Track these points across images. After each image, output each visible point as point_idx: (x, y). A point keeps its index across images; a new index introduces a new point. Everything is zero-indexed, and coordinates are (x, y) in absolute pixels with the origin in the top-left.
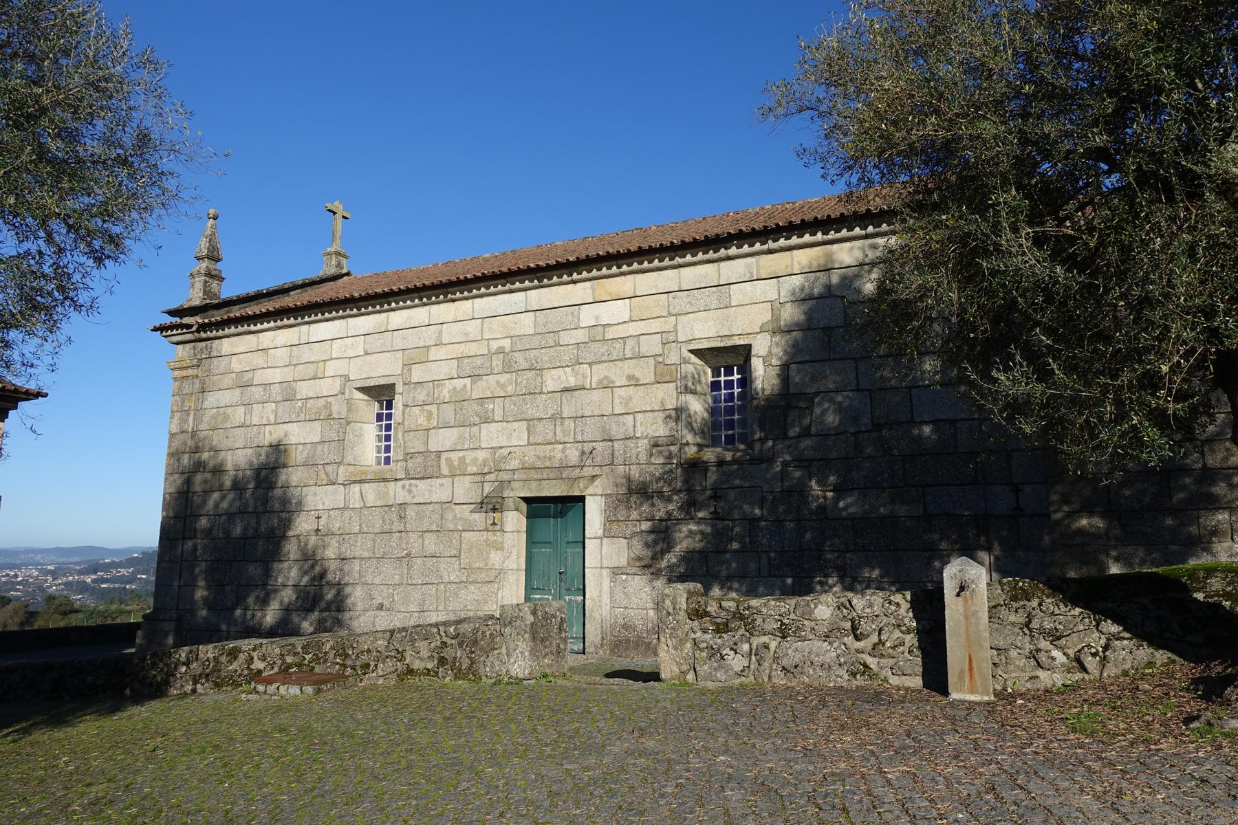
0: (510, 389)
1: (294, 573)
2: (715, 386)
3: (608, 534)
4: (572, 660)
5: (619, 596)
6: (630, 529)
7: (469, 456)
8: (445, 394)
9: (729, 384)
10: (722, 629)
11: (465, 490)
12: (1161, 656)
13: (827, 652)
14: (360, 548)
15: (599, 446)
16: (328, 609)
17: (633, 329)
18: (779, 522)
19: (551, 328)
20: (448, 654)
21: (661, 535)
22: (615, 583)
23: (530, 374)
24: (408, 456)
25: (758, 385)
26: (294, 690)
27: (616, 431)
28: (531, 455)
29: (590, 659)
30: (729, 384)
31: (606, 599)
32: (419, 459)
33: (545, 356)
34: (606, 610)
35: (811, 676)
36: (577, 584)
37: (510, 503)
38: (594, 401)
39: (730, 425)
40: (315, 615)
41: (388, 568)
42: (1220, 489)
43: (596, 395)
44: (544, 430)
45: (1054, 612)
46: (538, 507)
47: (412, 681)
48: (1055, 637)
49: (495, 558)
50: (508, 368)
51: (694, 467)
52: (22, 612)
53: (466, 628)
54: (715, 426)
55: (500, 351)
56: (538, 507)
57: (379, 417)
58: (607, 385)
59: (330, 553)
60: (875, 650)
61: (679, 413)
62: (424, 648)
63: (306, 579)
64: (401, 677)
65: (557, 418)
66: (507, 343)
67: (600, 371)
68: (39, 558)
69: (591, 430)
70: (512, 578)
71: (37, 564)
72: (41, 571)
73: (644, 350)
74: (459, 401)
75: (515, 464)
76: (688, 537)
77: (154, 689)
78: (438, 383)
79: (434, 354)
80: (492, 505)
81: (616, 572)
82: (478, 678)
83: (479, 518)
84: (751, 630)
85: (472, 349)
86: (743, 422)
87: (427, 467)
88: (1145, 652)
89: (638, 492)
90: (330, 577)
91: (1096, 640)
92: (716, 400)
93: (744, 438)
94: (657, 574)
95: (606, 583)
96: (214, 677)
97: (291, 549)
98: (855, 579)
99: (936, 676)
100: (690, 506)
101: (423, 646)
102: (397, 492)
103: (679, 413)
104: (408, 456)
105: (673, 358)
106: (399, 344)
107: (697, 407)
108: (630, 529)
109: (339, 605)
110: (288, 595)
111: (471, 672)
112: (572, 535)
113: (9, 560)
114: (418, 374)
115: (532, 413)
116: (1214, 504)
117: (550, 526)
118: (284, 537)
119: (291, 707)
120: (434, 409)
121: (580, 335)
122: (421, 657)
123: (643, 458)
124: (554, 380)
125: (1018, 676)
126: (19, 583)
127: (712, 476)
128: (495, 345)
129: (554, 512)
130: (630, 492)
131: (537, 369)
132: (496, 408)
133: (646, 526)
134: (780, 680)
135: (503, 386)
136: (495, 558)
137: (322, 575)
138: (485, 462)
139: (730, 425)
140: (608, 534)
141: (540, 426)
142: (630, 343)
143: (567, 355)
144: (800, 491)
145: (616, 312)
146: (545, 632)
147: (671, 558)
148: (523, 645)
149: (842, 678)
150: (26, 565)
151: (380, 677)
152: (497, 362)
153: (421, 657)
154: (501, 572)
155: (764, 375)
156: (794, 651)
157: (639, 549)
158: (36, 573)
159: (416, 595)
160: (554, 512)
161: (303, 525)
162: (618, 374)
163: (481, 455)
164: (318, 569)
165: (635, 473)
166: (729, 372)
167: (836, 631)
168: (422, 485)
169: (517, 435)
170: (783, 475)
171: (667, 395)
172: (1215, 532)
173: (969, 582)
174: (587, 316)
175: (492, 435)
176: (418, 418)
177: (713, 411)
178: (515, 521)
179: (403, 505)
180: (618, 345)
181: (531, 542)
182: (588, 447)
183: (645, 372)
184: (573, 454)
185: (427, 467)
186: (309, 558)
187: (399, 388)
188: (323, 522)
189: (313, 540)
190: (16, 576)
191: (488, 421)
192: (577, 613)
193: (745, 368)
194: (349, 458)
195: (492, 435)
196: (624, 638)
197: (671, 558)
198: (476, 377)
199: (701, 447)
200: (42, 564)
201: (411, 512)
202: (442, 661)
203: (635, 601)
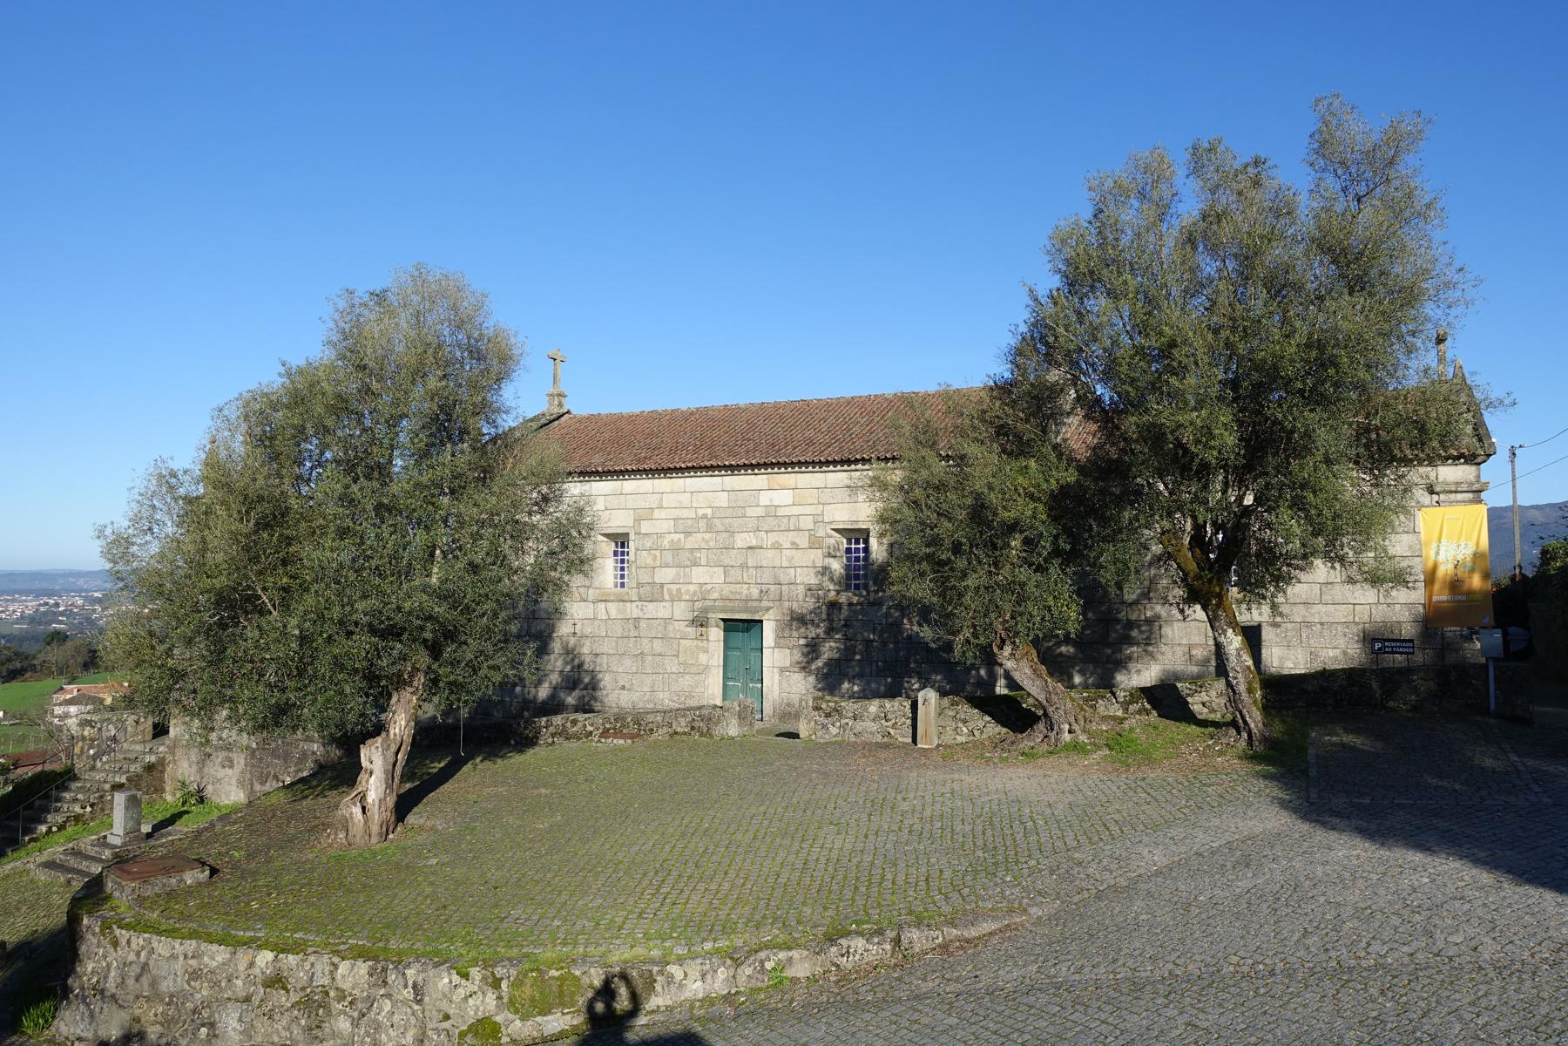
0: (712, 544)
1: (559, 663)
2: (848, 551)
3: (777, 646)
4: (758, 725)
5: (785, 685)
6: (793, 642)
7: (684, 588)
8: (666, 543)
9: (857, 550)
10: (828, 715)
11: (681, 611)
12: (1004, 730)
13: (874, 727)
14: (606, 647)
15: (772, 588)
16: (585, 688)
17: (796, 510)
18: (884, 643)
19: (740, 503)
20: (696, 724)
21: (812, 649)
22: (783, 677)
23: (725, 535)
24: (639, 585)
25: (873, 556)
26: (621, 742)
27: (783, 578)
28: (726, 590)
29: (767, 724)
30: (857, 550)
31: (776, 687)
32: (648, 588)
33: (736, 523)
34: (776, 694)
35: (866, 737)
36: (757, 676)
37: (712, 622)
38: (768, 558)
39: (857, 577)
40: (576, 693)
41: (627, 662)
42: (1135, 633)
43: (770, 554)
44: (735, 574)
45: (966, 710)
46: (731, 626)
47: (677, 737)
48: (965, 722)
49: (703, 658)
50: (710, 528)
51: (833, 606)
52: (84, 651)
53: (705, 712)
54: (848, 577)
55: (705, 516)
56: (731, 626)
57: (616, 553)
58: (777, 547)
59: (585, 650)
60: (893, 726)
61: (825, 570)
62: (683, 721)
63: (568, 668)
64: (671, 736)
65: (744, 566)
66: (709, 512)
67: (773, 537)
68: (81, 582)
69: (767, 577)
70: (714, 671)
71: (81, 590)
72: (86, 598)
73: (802, 526)
74: (676, 549)
75: (716, 595)
76: (829, 650)
77: (527, 742)
78: (660, 535)
79: (656, 514)
80: (700, 622)
81: (782, 670)
82: (711, 736)
83: (691, 631)
84: (841, 716)
85: (685, 514)
86: (865, 576)
87: (654, 594)
88: (999, 728)
89: (799, 620)
90: (586, 667)
91: (981, 724)
92: (849, 559)
93: (866, 587)
94: (810, 673)
95: (777, 676)
96: (563, 733)
97: (556, 646)
98: (927, 680)
99: (915, 741)
100: (830, 631)
101: (683, 721)
102: (633, 610)
103: (825, 570)
104: (639, 585)
105: (821, 533)
106: (630, 504)
107: (837, 566)
108: (793, 642)
109: (594, 686)
110: (555, 678)
111: (708, 734)
112: (754, 644)
113: (45, 585)
114: (645, 527)
115: (726, 562)
116: (1130, 641)
117: (739, 637)
118: (550, 636)
119: (621, 749)
120: (658, 553)
121: (759, 511)
122: (681, 725)
123: (801, 597)
124: (742, 540)
125: (948, 738)
126: (62, 614)
127: (845, 613)
128: (700, 512)
129: (741, 629)
130: (793, 619)
131: (731, 532)
132: (702, 556)
133: (802, 642)
134: (853, 739)
135: (707, 542)
136: (703, 658)
137: (580, 665)
138: (695, 593)
139: (857, 577)
140: (777, 646)
141: (732, 571)
142: (793, 520)
143: (751, 524)
144: (897, 625)
145: (783, 497)
146: (744, 715)
147: (819, 663)
148: (734, 721)
149: (879, 738)
150: (68, 591)
151: (661, 735)
152: (702, 524)
153: (681, 725)
154: (707, 667)
155: (878, 550)
156: (859, 726)
157: (798, 656)
158: (80, 602)
159: (648, 680)
160: (741, 629)
161: (564, 629)
162: (785, 540)
163: (692, 588)
164: (576, 662)
165: (795, 606)
166: (857, 542)
167: (875, 717)
168: (651, 606)
169: (718, 576)
170: (887, 615)
171: (817, 557)
172: (1130, 658)
173: (929, 698)
174: (764, 498)
175: (699, 575)
176: (646, 558)
177: (847, 568)
178: (716, 634)
179: (637, 619)
180: (785, 520)
181: (727, 647)
182: (764, 588)
183: (803, 541)
184: (755, 592)
185: (654, 594)
186: (569, 652)
187: (632, 537)
188: (578, 627)
189: (572, 641)
190: (57, 605)
191: (696, 564)
192: (757, 695)
193: (866, 541)
194: (596, 584)
195: (699, 575)
196: (789, 713)
197: (819, 663)
198: (688, 533)
199: (838, 592)
200: (86, 591)
201: (643, 624)
202: (693, 728)
203: (795, 689)
